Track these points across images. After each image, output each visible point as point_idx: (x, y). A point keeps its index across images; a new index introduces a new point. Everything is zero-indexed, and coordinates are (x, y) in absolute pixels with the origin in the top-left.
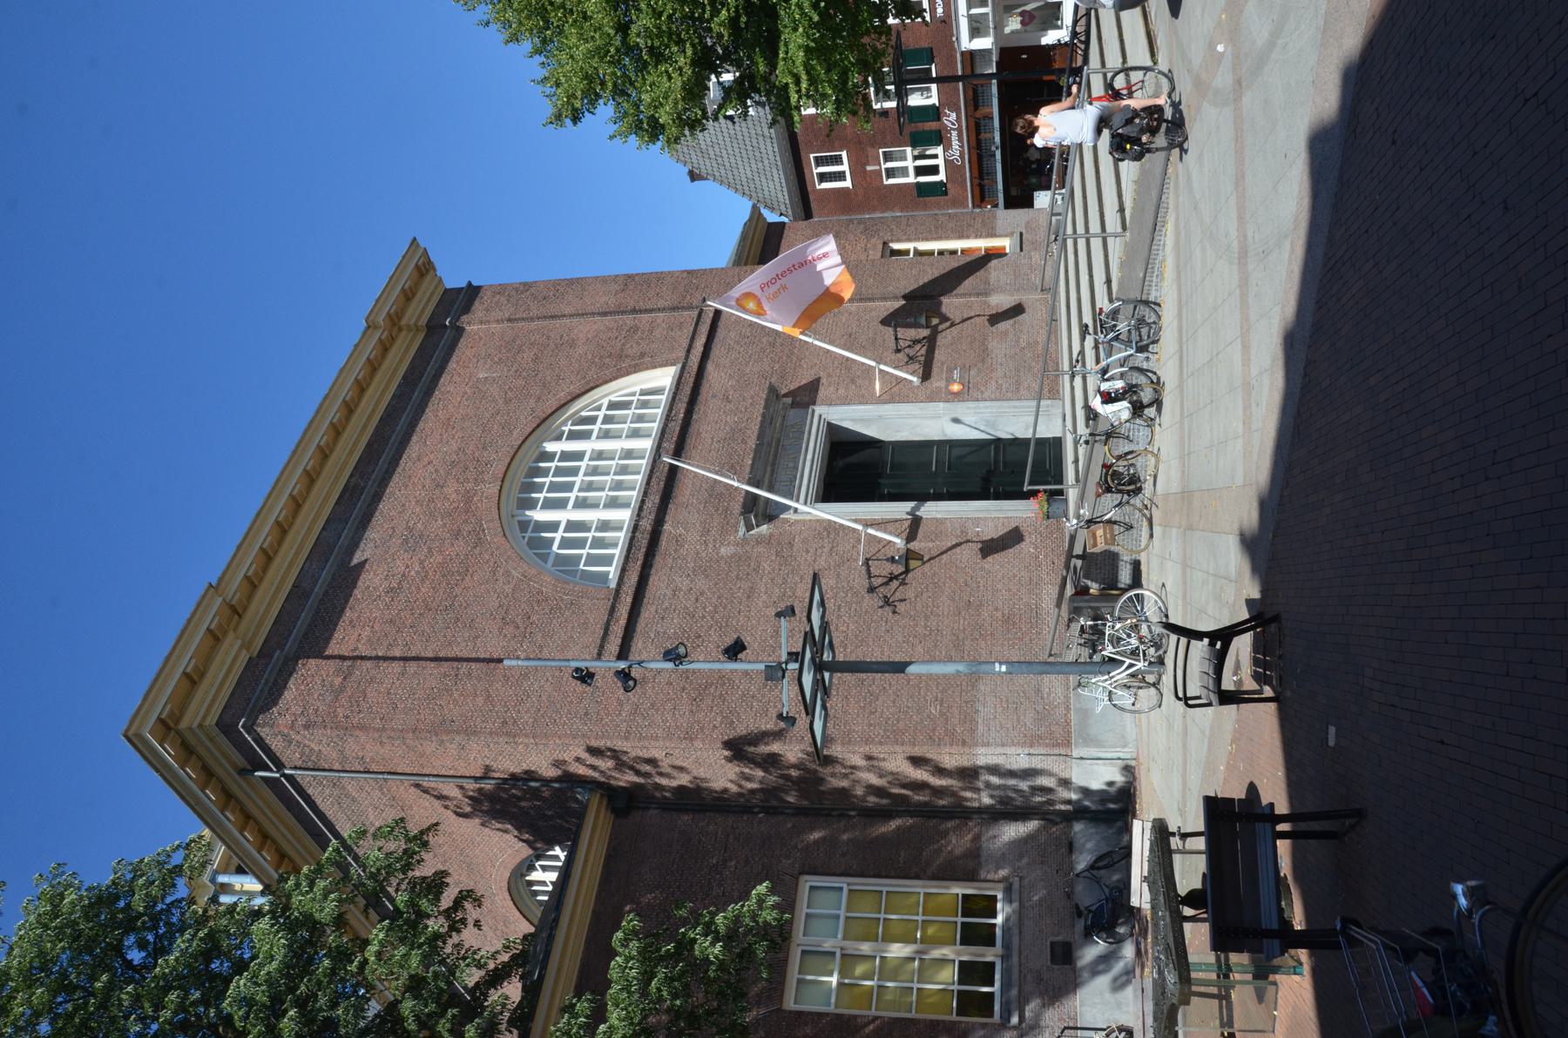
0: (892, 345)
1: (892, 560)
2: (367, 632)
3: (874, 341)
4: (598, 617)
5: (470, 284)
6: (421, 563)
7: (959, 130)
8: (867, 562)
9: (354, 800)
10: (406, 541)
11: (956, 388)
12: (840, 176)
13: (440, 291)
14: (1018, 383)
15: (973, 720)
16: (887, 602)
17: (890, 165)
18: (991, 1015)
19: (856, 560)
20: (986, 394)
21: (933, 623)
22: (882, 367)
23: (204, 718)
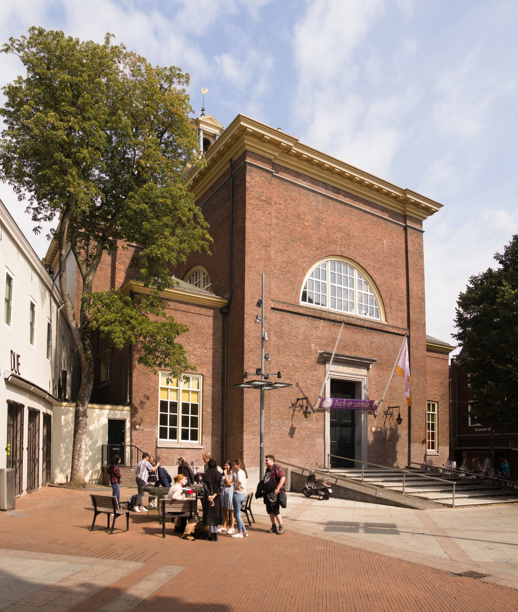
0: (391, 406)
2: (282, 207)
3: (393, 398)
10: (318, 219)
16: (293, 405)
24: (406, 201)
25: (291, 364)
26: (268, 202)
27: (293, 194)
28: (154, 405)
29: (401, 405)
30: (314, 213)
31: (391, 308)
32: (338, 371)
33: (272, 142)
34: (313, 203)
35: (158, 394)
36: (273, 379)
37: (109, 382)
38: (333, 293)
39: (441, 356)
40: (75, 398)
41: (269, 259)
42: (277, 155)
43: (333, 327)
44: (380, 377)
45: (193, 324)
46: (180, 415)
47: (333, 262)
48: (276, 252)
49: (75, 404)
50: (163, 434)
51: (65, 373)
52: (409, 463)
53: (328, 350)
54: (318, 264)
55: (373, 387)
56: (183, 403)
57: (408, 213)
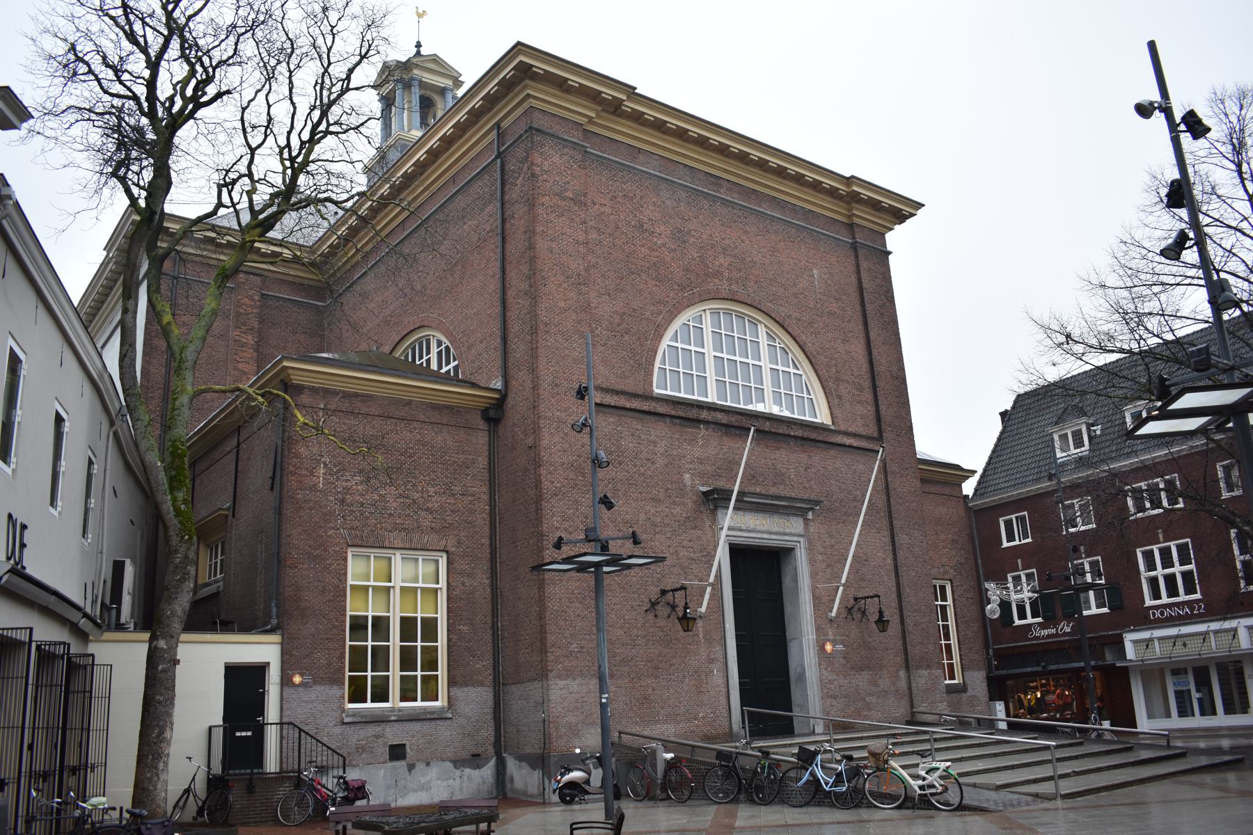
0: (860, 595)
1: (686, 607)
2: (608, 210)
3: (863, 580)
4: (629, 385)
5: (890, 253)
6: (664, 245)
7: (1057, 635)
8: (683, 588)
9: (482, 210)
10: (680, 231)
11: (829, 647)
12: (1011, 537)
13: (882, 230)
14: (835, 697)
15: (568, 676)
16: (654, 604)
17: (1024, 578)
18: (350, 702)
19: (686, 579)
20: (824, 672)
21: (640, 641)
22: (841, 588)
23: (535, 97)
24: (854, 198)
25: (642, 517)
26: (580, 201)
27: (627, 187)
28: (335, 627)
29: (881, 590)
30: (671, 221)
31: (840, 397)
32: (744, 527)
33: (583, 92)
34: (668, 202)
35: (345, 601)
36: (626, 547)
37: (221, 584)
38: (720, 371)
39: (947, 490)
40: (150, 619)
41: (587, 308)
42: (593, 115)
43: (725, 439)
44: (831, 536)
45: (424, 445)
46: (395, 642)
47: (716, 313)
48: (600, 295)
49: (147, 636)
50: (357, 696)
51: (118, 568)
52: (913, 714)
53: (721, 484)
54: (686, 316)
55: (820, 557)
56: (402, 618)
57: (856, 220)
